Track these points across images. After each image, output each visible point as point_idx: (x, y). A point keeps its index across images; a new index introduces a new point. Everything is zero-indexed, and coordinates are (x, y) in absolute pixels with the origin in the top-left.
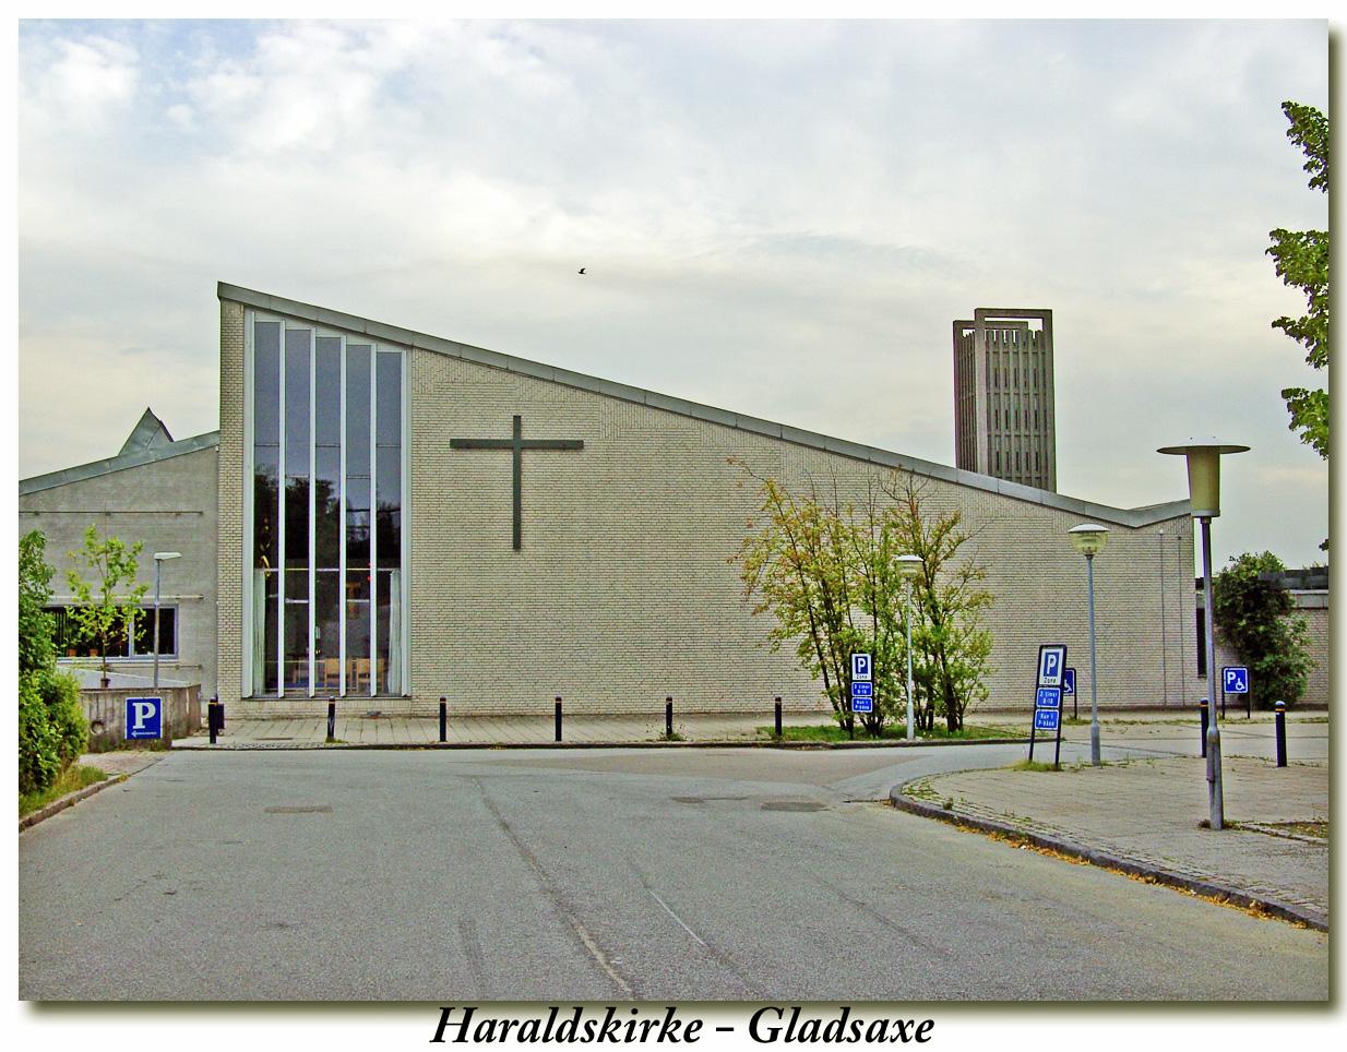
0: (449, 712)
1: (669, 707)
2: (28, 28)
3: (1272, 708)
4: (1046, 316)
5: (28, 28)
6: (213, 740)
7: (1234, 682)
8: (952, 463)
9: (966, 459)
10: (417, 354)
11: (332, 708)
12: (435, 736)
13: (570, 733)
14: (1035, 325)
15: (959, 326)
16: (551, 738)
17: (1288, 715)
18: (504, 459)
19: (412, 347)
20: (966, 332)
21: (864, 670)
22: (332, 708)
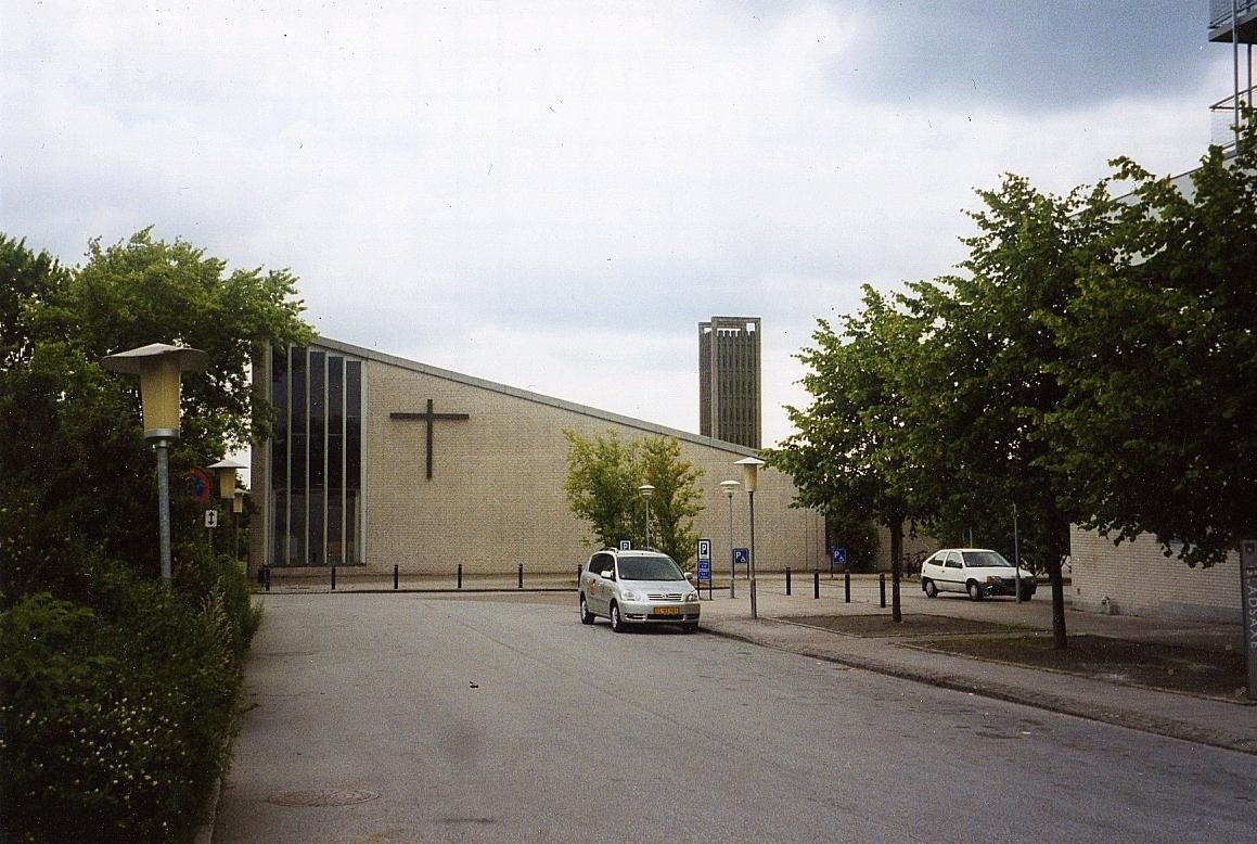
0: (524, 571)
1: (521, 570)
2: (700, 324)
3: (844, 572)
4: (757, 321)
5: (700, 324)
6: (333, 588)
7: (740, 558)
8: (698, 433)
9: (705, 430)
10: (370, 363)
11: (334, 571)
12: (392, 587)
13: (465, 584)
14: (750, 327)
15: (702, 325)
16: (456, 587)
17: (851, 576)
18: (420, 427)
19: (367, 359)
20: (707, 330)
21: (705, 552)
22: (334, 571)
